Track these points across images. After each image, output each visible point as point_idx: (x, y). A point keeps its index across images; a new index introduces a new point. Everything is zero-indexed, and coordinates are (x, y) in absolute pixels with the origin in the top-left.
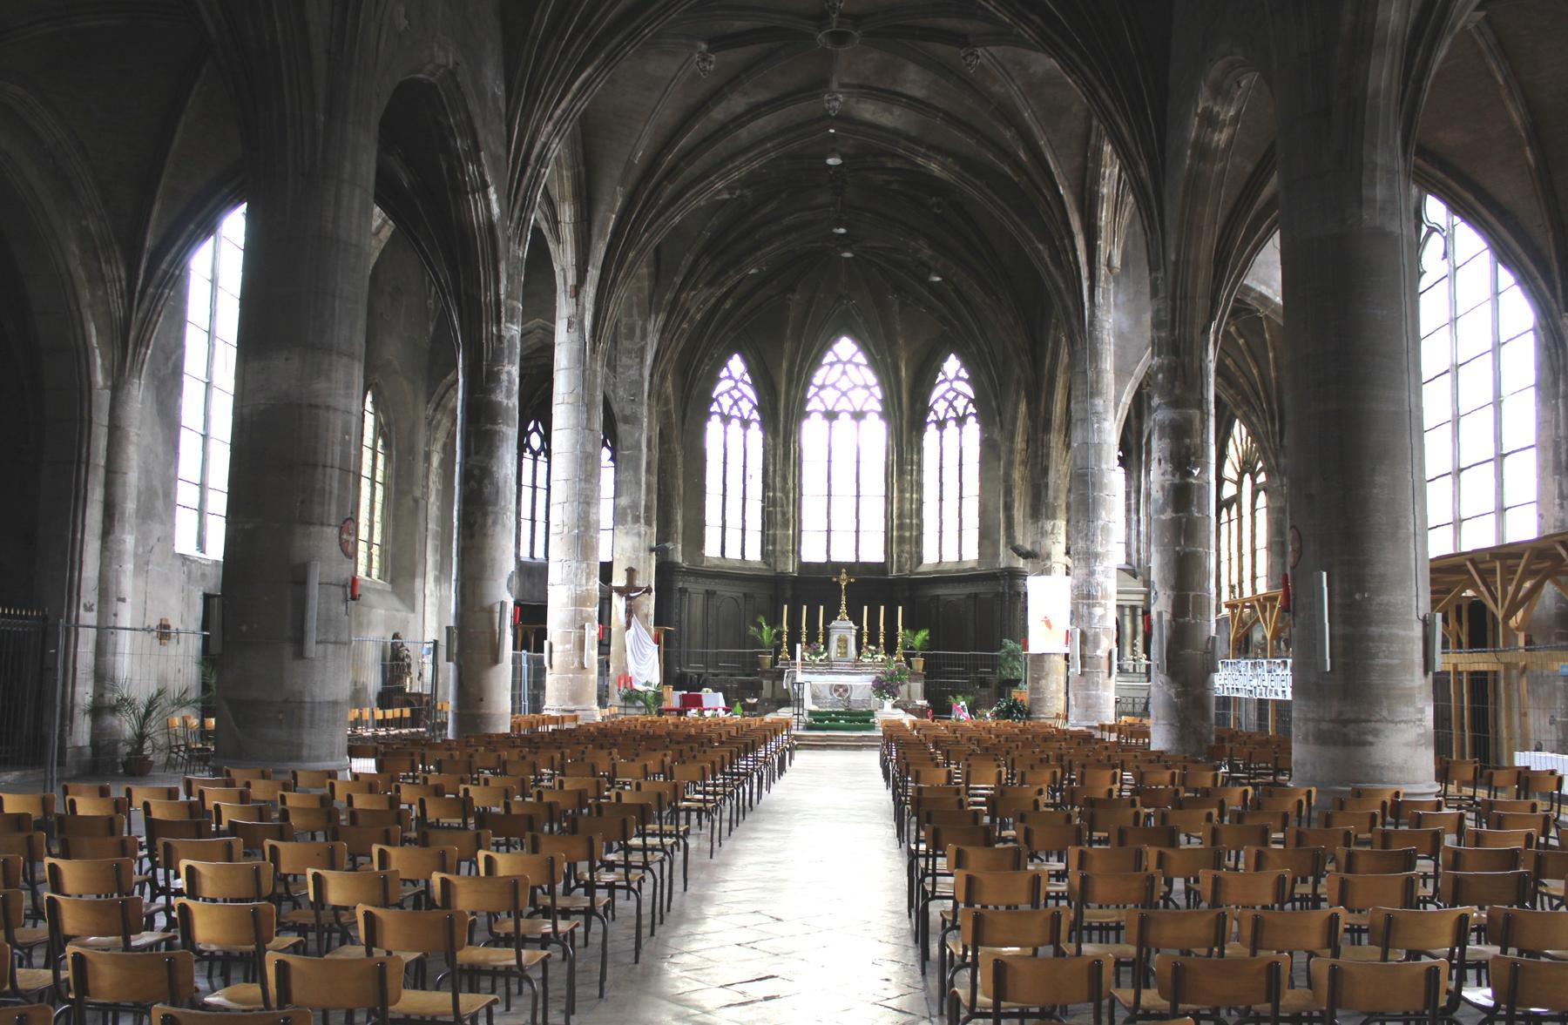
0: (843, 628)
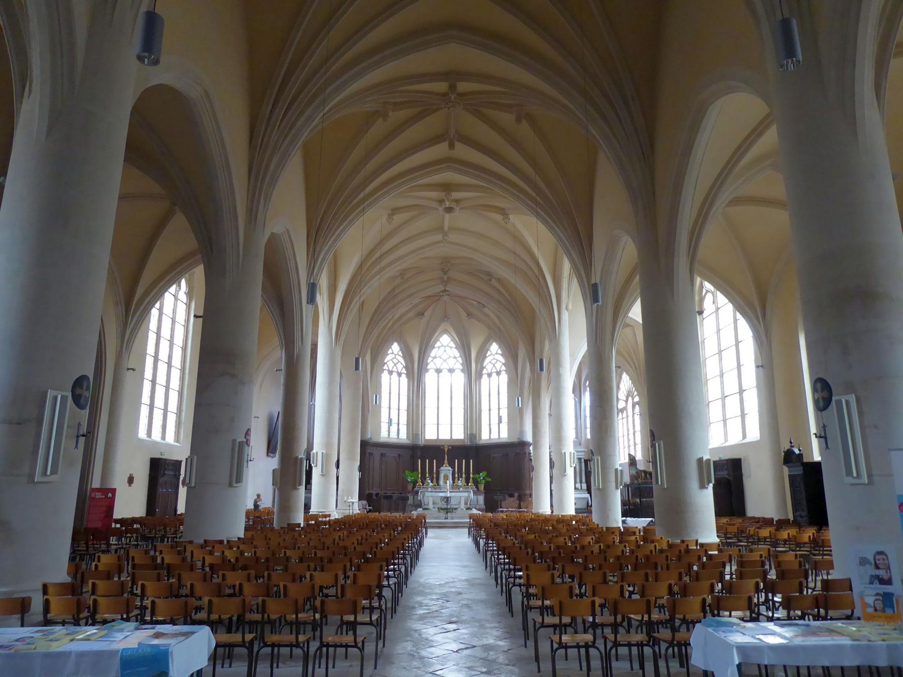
0: (446, 470)
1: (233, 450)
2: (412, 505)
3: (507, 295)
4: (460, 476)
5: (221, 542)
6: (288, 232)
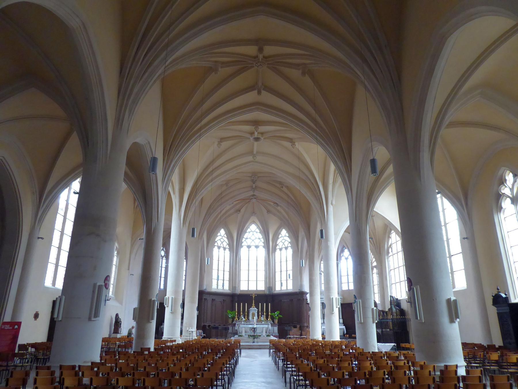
0: (253, 310)
1: (94, 292)
2: (231, 333)
3: (293, 198)
4: (262, 314)
5: (74, 367)
6: (149, 143)
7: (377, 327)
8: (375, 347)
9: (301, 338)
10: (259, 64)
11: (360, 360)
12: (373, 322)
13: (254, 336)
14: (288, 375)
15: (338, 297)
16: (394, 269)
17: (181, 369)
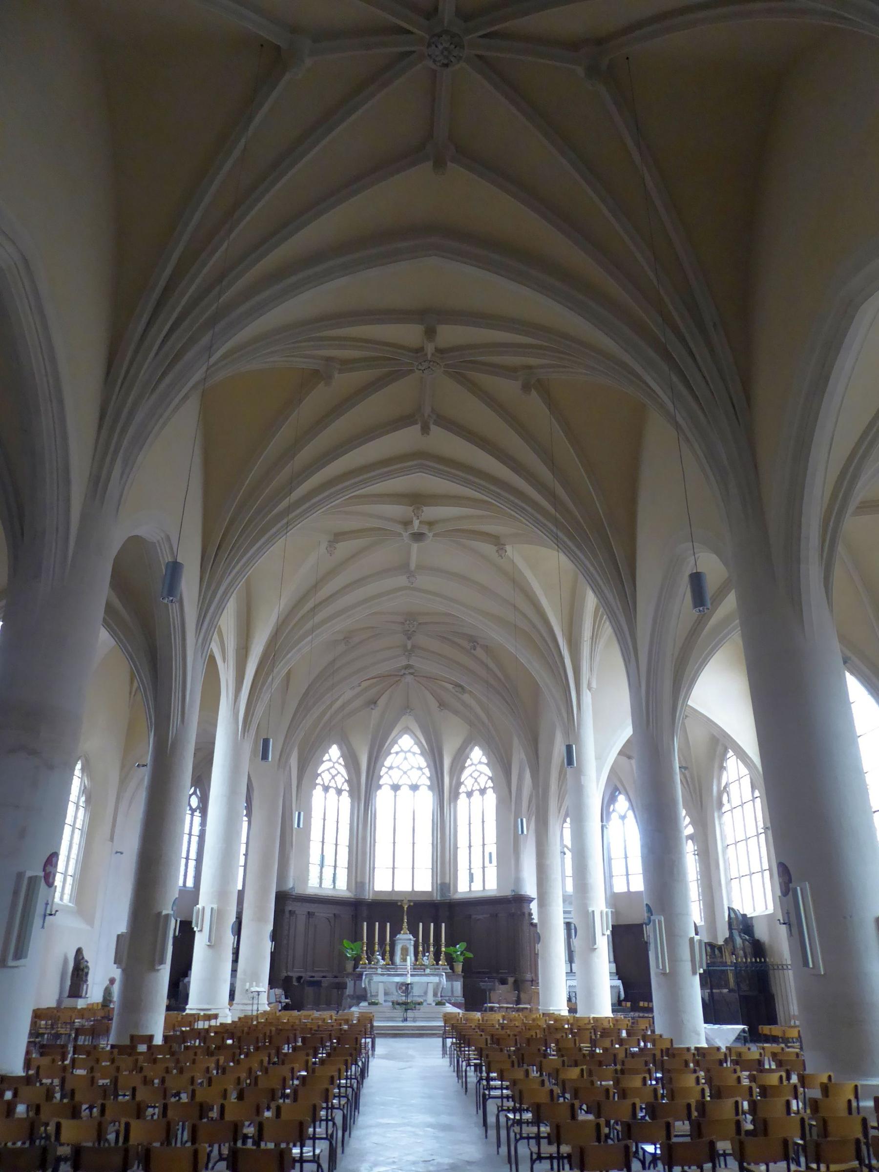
0: (405, 939)
1: (16, 893)
2: (352, 997)
4: (426, 950)
6: (168, 538)
7: (703, 986)
8: (698, 1034)
9: (518, 1010)
10: (426, 365)
11: (669, 1071)
12: (694, 973)
13: (406, 1004)
14: (492, 1107)
15: (605, 910)
16: (736, 843)
17: (225, 1094)
